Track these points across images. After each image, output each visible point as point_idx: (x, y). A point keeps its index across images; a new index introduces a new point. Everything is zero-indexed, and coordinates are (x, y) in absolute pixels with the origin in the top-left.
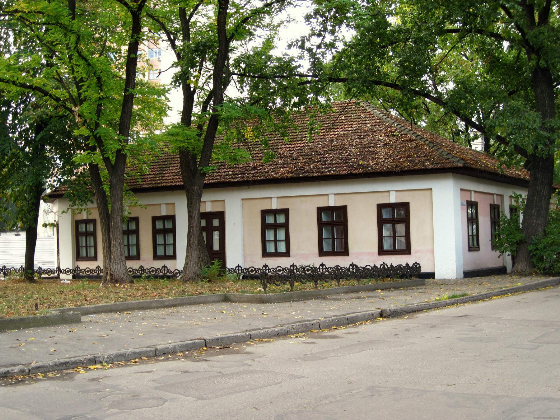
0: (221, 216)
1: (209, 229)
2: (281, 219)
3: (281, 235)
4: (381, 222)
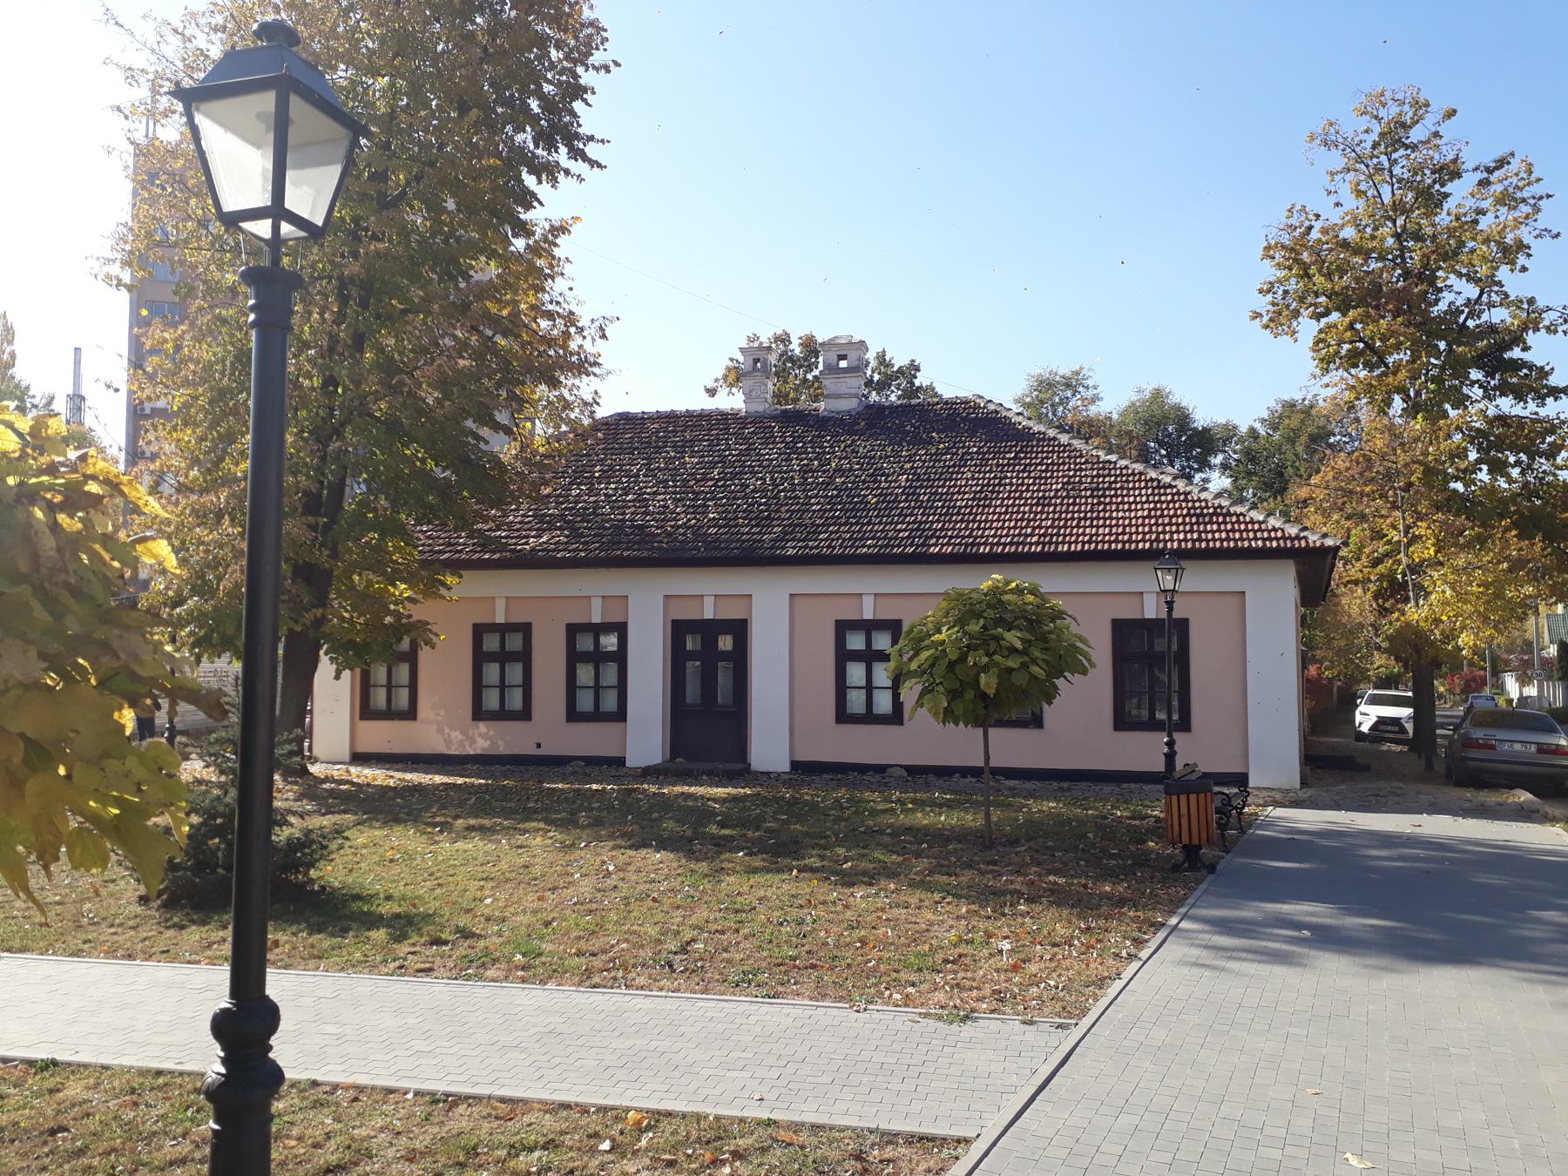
3: (515, 673)
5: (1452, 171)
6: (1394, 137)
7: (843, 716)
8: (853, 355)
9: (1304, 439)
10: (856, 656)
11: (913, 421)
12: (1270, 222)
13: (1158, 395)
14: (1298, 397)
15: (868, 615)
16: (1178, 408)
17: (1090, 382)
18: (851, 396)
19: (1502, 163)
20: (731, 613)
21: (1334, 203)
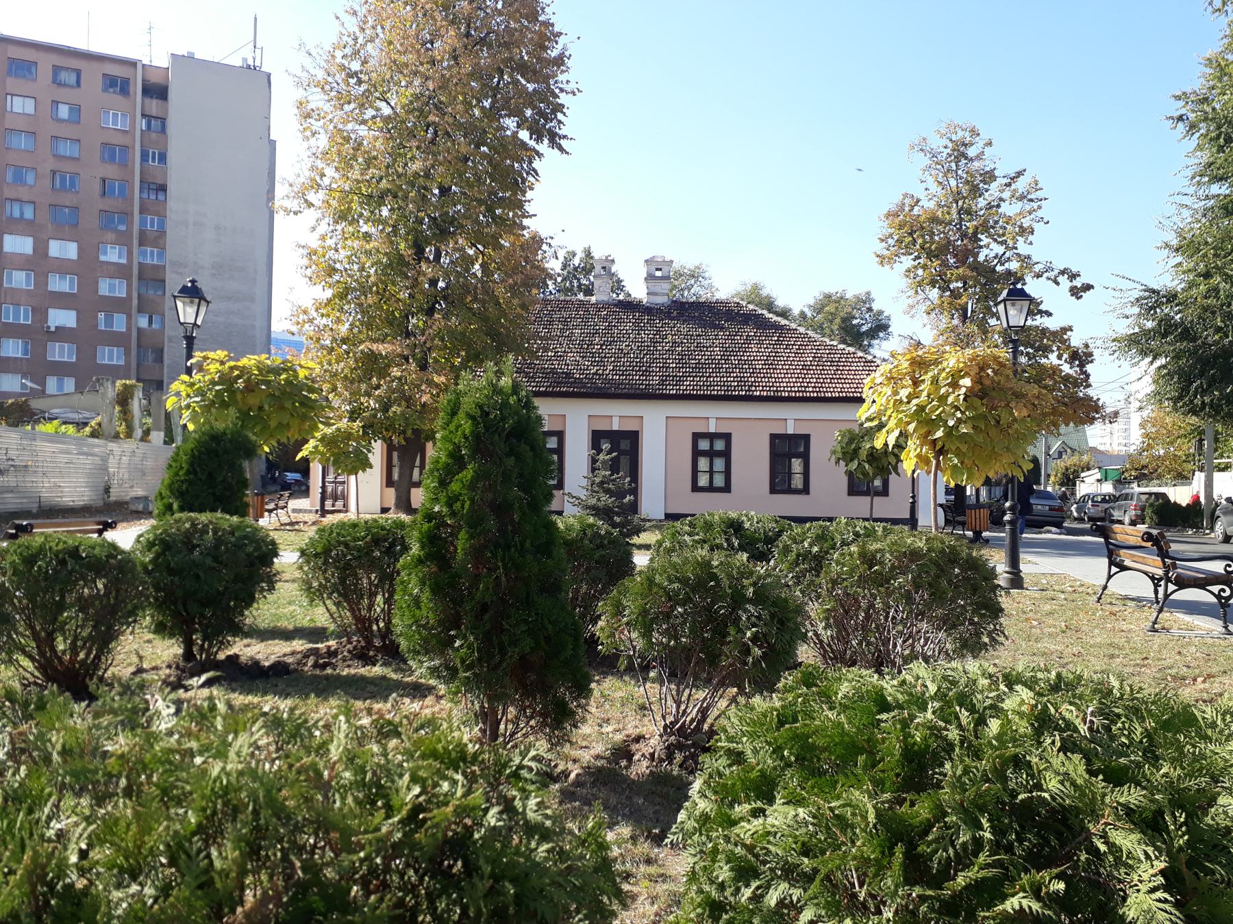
2: (719, 445)
3: (719, 464)
5: (990, 176)
6: (959, 153)
7: (695, 488)
8: (665, 269)
9: (838, 321)
10: (704, 453)
11: (749, 319)
12: (891, 200)
13: (756, 288)
14: (833, 291)
15: (712, 430)
16: (769, 297)
17: (707, 275)
18: (663, 294)
19: (1019, 174)
20: (630, 426)
21: (929, 193)
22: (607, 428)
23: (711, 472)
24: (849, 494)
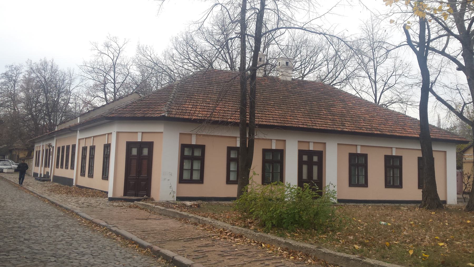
0: (321, 155)
1: (310, 164)
2: (197, 153)
3: (197, 166)
4: (183, 158)
10: (188, 158)
22: (355, 152)
23: (192, 170)
24: (386, 187)
